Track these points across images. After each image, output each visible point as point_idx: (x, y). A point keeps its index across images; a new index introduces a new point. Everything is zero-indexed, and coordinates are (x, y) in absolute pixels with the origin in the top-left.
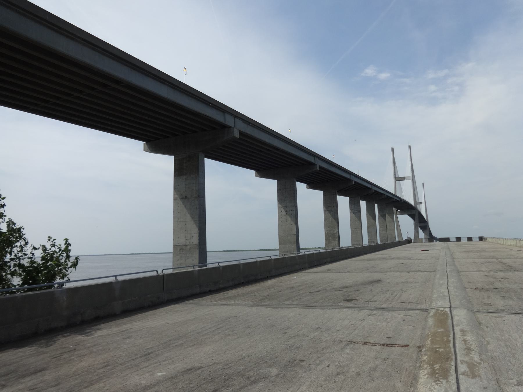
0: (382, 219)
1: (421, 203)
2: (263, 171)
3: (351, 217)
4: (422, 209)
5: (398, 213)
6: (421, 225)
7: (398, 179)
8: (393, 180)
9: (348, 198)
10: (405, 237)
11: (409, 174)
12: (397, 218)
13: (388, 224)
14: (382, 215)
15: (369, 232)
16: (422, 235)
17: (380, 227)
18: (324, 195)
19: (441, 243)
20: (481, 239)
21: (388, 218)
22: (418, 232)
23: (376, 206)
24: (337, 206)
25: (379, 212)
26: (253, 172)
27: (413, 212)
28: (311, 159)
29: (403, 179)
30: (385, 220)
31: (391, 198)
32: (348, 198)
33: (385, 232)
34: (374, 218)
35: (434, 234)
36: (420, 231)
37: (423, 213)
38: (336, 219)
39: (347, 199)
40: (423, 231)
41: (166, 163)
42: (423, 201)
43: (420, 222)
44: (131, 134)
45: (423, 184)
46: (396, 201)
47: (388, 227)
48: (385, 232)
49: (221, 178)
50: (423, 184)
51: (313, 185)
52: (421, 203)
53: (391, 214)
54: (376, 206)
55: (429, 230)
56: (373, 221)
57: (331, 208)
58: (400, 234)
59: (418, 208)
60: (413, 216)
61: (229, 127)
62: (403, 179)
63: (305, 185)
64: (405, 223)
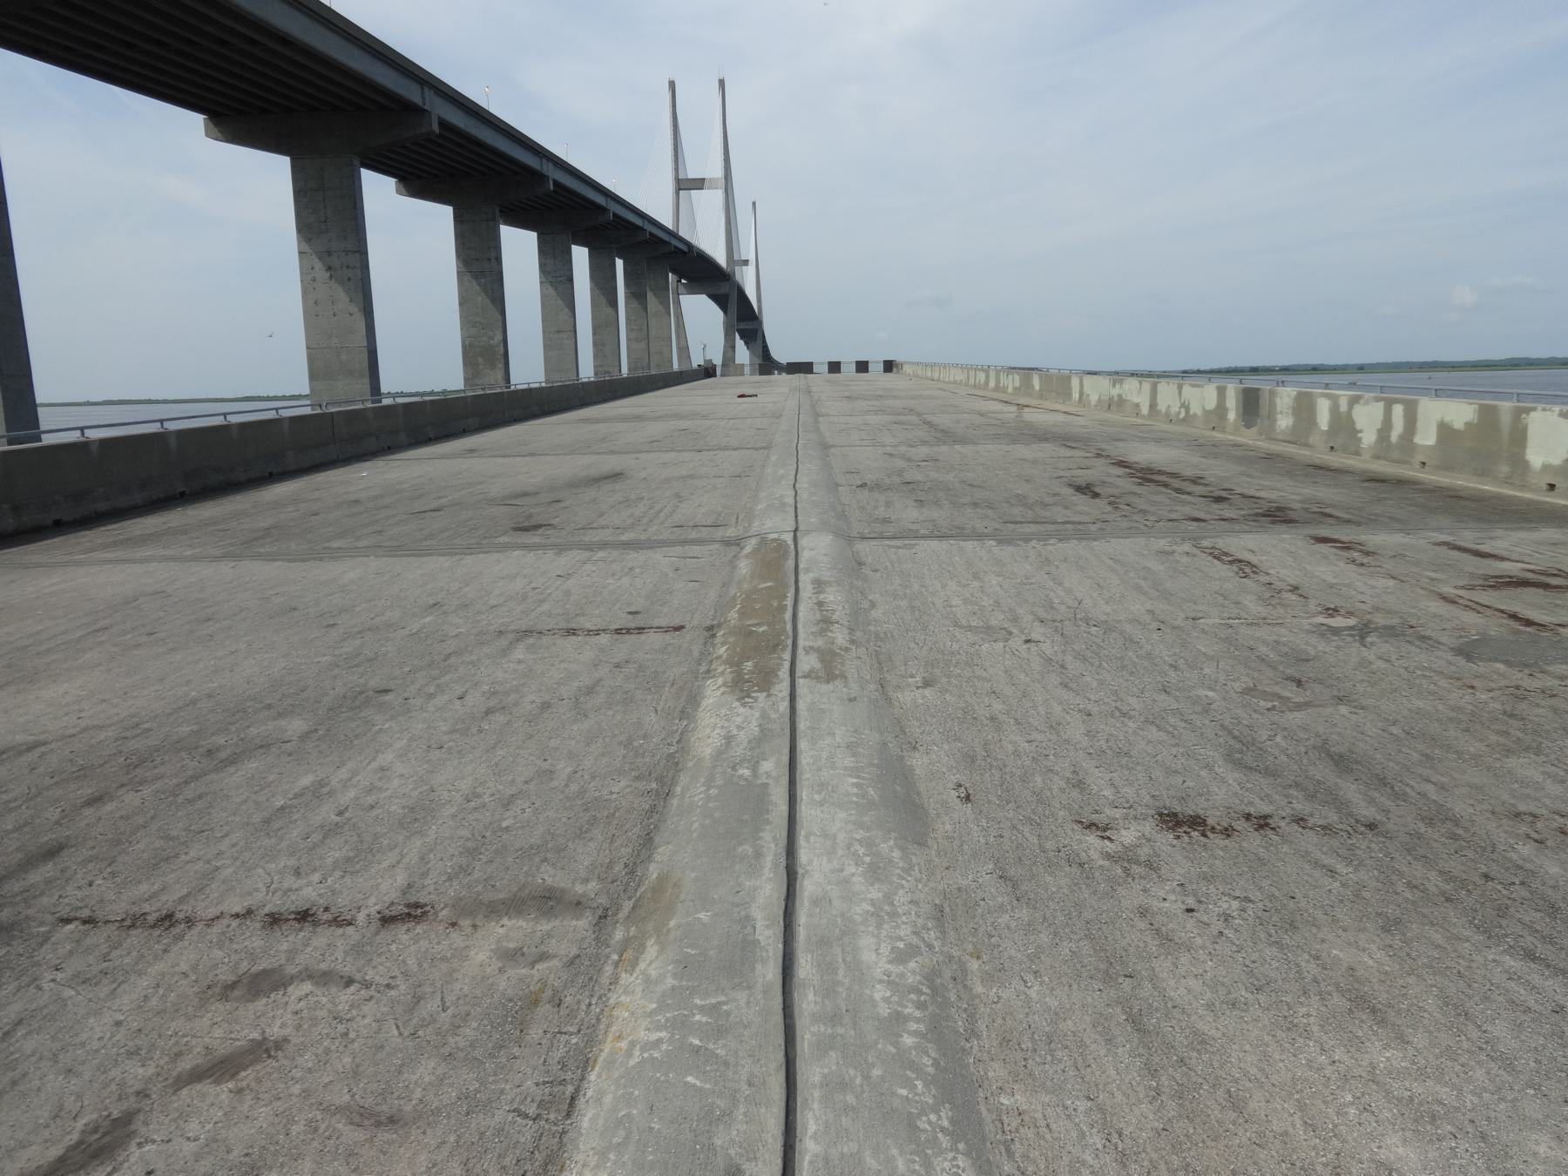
0: (635, 304)
1: (746, 262)
5: (681, 289)
6: (743, 326)
7: (685, 185)
9: (450, 209)
10: (697, 360)
11: (715, 171)
12: (677, 303)
13: (653, 322)
15: (598, 345)
16: (743, 353)
17: (629, 330)
18: (458, 219)
21: (652, 301)
22: (733, 347)
23: (619, 263)
24: (499, 260)
25: (627, 285)
27: (724, 289)
29: (699, 184)
32: (534, 235)
33: (643, 345)
34: (613, 303)
36: (740, 344)
42: (752, 257)
43: (740, 319)
47: (653, 332)
51: (521, 220)
52: (746, 262)
54: (619, 263)
56: (610, 310)
57: (480, 265)
58: (684, 351)
59: (738, 277)
60: (721, 301)
62: (699, 184)
64: (701, 318)
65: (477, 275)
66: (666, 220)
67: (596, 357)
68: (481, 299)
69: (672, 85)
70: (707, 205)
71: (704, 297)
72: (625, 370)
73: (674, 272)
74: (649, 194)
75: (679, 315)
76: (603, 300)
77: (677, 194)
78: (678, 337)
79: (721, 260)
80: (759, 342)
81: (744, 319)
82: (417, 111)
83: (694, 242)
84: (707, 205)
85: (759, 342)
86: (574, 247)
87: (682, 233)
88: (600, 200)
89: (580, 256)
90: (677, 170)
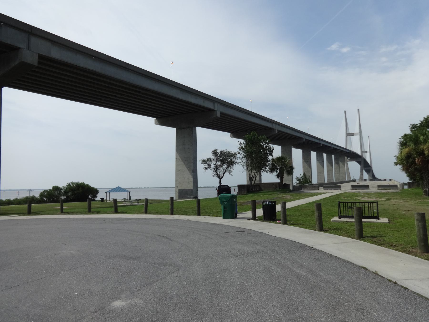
0: (336, 165)
1: (366, 152)
2: (163, 120)
3: (317, 165)
4: (367, 158)
5: (348, 160)
6: (366, 169)
7: (348, 135)
8: (345, 135)
9: (175, 129)
10: (352, 179)
11: (357, 131)
12: (347, 163)
13: (341, 169)
14: (337, 163)
15: (328, 175)
16: (366, 176)
17: (335, 171)
18: (303, 152)
19: (8, 198)
20: (390, 180)
21: (341, 164)
22: (363, 175)
23: (333, 156)
24: (311, 159)
25: (335, 161)
26: (228, 134)
27: (360, 160)
28: (209, 105)
29: (353, 134)
30: (339, 166)
31: (318, 143)
32: (175, 129)
33: (338, 175)
34: (332, 166)
35: (377, 176)
36: (365, 173)
37: (368, 160)
38: (310, 167)
39: (280, 147)
40: (367, 173)
41: (172, 131)
42: (368, 150)
43: (365, 167)
44: (61, 95)
45: (369, 137)
46: (347, 152)
47: (341, 171)
48: (338, 175)
49: (210, 140)
50: (369, 137)
51: (297, 147)
52: (366, 152)
53: (343, 161)
54: (333, 156)
55: (373, 173)
56: (331, 167)
57: (307, 159)
58: (349, 176)
59: (364, 156)
60: (359, 163)
61: (17, 49)
62: (353, 134)
63: (153, 119)
64: (354, 167)
65: (306, 162)
66: (344, 146)
67: (190, 215)
68: (307, 167)
69: (345, 112)
70: (355, 139)
71: (355, 162)
72: (334, 181)
73: (346, 156)
74: (339, 141)
75: (347, 167)
76: (329, 165)
77: (347, 137)
78: (347, 172)
79: (359, 153)
80: (371, 173)
81: (366, 166)
82: (320, 144)
83: (352, 150)
84: (355, 139)
85: (371, 173)
86: (311, 152)
87: (348, 148)
88: (330, 145)
89: (314, 154)
90: (346, 131)
